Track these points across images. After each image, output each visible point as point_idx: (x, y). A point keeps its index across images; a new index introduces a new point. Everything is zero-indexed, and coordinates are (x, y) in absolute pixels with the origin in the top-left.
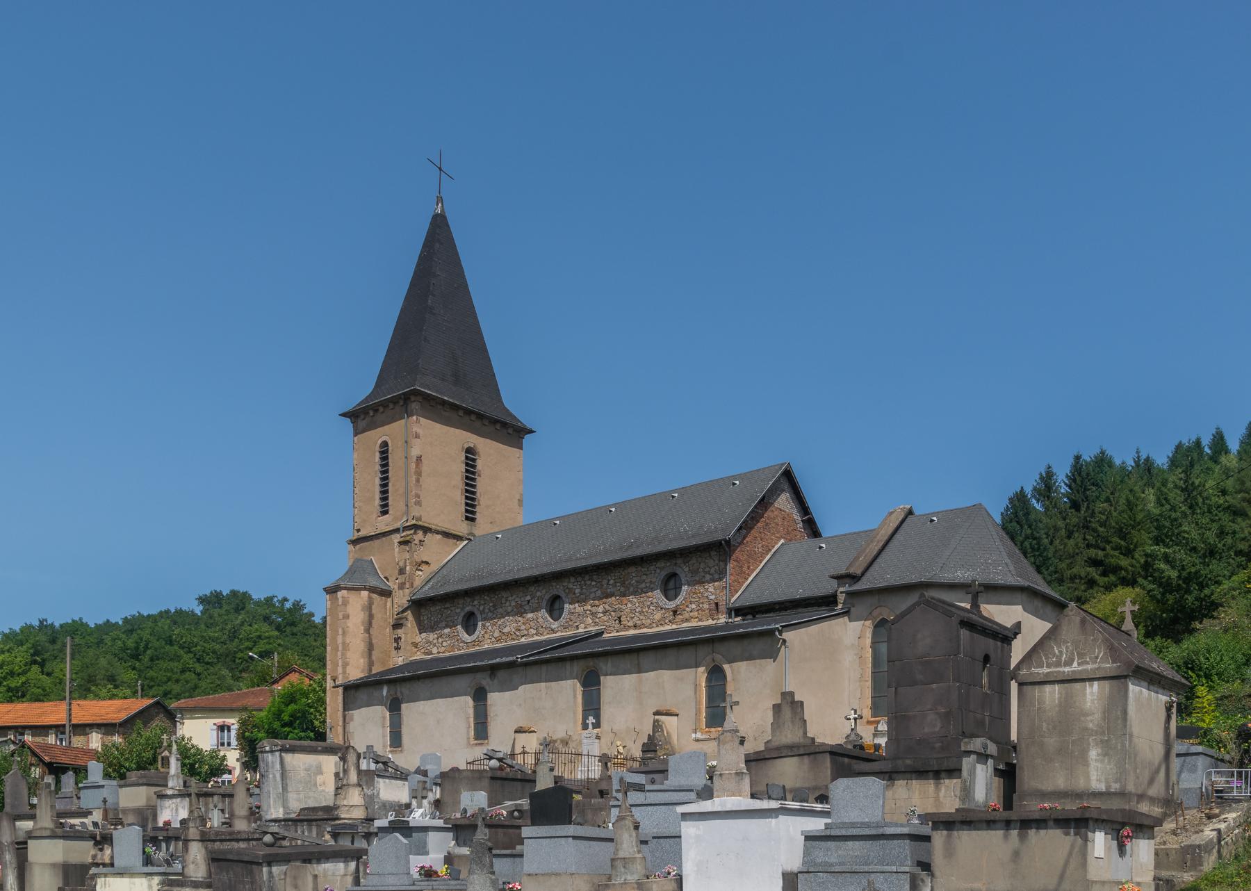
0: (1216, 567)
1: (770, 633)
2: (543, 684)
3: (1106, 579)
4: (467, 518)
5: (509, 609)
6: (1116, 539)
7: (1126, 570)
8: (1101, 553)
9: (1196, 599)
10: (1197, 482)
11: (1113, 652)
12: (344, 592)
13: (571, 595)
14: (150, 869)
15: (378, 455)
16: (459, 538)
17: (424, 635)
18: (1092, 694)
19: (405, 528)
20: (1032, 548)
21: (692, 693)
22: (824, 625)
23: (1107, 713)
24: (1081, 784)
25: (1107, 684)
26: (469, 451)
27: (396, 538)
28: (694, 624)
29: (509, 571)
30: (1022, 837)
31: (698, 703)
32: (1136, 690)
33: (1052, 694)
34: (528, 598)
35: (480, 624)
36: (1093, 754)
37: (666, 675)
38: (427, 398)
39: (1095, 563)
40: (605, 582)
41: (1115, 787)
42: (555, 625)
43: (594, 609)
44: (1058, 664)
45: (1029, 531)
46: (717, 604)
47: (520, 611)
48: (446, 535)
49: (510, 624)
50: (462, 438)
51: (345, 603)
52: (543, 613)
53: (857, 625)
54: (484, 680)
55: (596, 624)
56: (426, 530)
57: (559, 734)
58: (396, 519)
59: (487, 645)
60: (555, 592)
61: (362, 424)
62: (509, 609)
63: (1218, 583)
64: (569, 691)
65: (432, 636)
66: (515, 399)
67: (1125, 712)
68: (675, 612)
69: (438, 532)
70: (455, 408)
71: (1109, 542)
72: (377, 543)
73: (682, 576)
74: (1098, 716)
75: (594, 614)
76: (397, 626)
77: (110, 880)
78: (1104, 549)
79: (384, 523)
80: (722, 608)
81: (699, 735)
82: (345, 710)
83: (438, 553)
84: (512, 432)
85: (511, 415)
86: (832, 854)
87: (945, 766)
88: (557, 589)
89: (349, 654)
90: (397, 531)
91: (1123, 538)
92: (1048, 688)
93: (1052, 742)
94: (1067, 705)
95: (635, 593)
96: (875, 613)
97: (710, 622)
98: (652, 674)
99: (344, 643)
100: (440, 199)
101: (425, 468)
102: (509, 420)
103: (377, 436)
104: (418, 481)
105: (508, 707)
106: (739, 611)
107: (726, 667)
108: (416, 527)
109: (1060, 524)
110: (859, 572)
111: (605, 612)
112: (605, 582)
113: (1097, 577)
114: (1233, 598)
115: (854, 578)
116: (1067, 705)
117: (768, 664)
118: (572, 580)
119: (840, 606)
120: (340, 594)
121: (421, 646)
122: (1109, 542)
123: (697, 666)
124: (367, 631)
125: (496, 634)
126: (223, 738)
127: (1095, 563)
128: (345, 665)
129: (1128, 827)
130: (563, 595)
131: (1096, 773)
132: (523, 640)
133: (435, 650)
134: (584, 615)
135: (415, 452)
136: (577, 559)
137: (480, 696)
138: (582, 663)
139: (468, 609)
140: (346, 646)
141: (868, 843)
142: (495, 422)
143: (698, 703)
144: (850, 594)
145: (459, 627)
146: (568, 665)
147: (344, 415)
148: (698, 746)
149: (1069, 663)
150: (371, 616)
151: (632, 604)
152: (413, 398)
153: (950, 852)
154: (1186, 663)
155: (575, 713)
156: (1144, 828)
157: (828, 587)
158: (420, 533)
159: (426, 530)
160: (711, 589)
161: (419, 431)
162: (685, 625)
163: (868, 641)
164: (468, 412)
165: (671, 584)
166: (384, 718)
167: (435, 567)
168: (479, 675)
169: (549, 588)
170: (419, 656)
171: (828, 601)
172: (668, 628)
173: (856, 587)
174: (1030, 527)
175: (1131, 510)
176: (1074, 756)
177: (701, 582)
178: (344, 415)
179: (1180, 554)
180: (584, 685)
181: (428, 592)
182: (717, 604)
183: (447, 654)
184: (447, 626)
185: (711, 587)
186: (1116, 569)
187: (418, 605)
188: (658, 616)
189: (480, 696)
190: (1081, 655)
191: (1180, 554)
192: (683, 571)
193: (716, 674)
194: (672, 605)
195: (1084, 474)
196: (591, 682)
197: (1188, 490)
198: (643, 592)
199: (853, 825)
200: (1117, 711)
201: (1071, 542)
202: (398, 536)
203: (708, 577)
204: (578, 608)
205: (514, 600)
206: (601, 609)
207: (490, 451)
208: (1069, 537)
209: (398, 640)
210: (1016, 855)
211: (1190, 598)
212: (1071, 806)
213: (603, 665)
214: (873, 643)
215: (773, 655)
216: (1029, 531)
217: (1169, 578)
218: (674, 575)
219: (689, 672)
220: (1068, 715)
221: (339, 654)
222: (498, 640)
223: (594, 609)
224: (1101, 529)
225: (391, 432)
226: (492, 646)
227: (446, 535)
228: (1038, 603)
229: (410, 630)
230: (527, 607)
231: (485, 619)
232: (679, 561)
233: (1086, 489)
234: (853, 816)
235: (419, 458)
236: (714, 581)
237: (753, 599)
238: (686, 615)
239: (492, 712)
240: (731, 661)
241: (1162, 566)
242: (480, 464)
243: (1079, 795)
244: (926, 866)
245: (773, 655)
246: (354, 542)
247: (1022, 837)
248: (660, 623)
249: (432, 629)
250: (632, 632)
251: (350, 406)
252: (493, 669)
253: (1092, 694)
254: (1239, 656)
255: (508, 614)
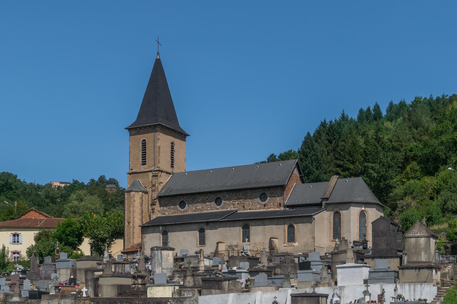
0: (391, 172)
1: (311, 216)
2: (228, 228)
3: (344, 173)
4: (172, 167)
5: (199, 201)
6: (347, 157)
7: (353, 170)
8: (342, 162)
9: (384, 184)
10: (381, 136)
11: (427, 231)
12: (133, 192)
13: (225, 198)
14: (169, 284)
15: (141, 145)
16: (170, 174)
17: (162, 208)
18: (422, 240)
19: (154, 171)
20: (315, 160)
21: (283, 233)
22: (321, 213)
23: (426, 244)
24: (420, 260)
25: (426, 238)
26: (172, 143)
27: (150, 174)
28: (272, 209)
29: (199, 188)
30: (419, 271)
31: (285, 235)
32: (432, 239)
33: (413, 240)
34: (207, 198)
35: (187, 205)
36: (423, 253)
37: (274, 227)
38: (162, 126)
39: (339, 166)
40: (238, 194)
41: (428, 260)
42: (218, 207)
43: (234, 203)
44: (415, 233)
45: (314, 153)
46: (280, 204)
47: (204, 202)
48: (167, 173)
49: (199, 206)
50: (171, 139)
51: (134, 196)
52: (214, 203)
53: (329, 213)
54: (204, 226)
55: (234, 207)
56: (162, 171)
57: (234, 243)
58: (149, 167)
59: (190, 213)
60: (218, 196)
61: (133, 132)
62: (199, 201)
63: (391, 178)
64: (238, 231)
65: (165, 208)
66: (183, 125)
67: (430, 244)
68: (265, 205)
69: (165, 172)
70: (169, 129)
71: (345, 158)
72: (141, 175)
73: (268, 195)
74: (424, 245)
75: (234, 205)
76: (153, 204)
77: (155, 288)
78: (343, 161)
79: (143, 168)
80: (282, 205)
81: (285, 245)
82: (142, 234)
83: (164, 179)
84: (182, 136)
85: (182, 130)
86: (374, 275)
87: (387, 256)
88: (220, 195)
89: (135, 214)
90: (151, 171)
91: (351, 157)
92: (412, 239)
93: (413, 251)
94: (416, 242)
95: (250, 199)
96: (335, 209)
97: (278, 209)
98: (269, 226)
99: (133, 210)
100: (158, 54)
101: (161, 150)
102: (182, 132)
103: (142, 137)
104: (159, 155)
105: (212, 235)
106: (288, 206)
107: (295, 225)
108: (159, 171)
109: (325, 149)
110: (328, 197)
111: (238, 204)
112: (238, 194)
113: (340, 172)
114: (398, 185)
115: (327, 199)
116: (416, 242)
117: (309, 225)
118: (225, 193)
119: (323, 207)
120: (131, 193)
121: (160, 212)
122: (345, 158)
123: (285, 224)
124: (141, 206)
125: (194, 209)
126: (15, 239)
127: (339, 166)
128: (134, 218)
129: (438, 269)
130: (222, 198)
131: (423, 258)
132: (205, 211)
133: (167, 213)
134: (230, 204)
135: (158, 144)
136: (227, 186)
137: (202, 231)
138: (243, 222)
139: (182, 200)
140: (134, 211)
141: (384, 273)
142: (179, 133)
143: (285, 235)
144: (326, 204)
145: (178, 206)
146: (237, 223)
147: (126, 129)
148: (285, 248)
149: (417, 233)
150: (142, 201)
151: (248, 202)
152: (158, 126)
153: (403, 274)
154: (405, 220)
155: (240, 237)
156: (439, 269)
157: (319, 201)
158: (160, 172)
159: (162, 171)
160: (278, 199)
161: (160, 137)
162: (269, 209)
163: (332, 217)
164: (172, 130)
165: (263, 196)
166: (160, 237)
167: (164, 184)
168: (202, 224)
169: (217, 196)
170: (160, 215)
171: (320, 205)
172: (262, 210)
173: (328, 202)
174: (314, 151)
175: (354, 146)
176: (418, 254)
177: (274, 197)
178: (126, 129)
179: (377, 166)
180: (243, 229)
181: (163, 193)
182: (280, 204)
183: (172, 215)
184: (172, 205)
185: (278, 198)
186: (348, 169)
187: (160, 198)
188: (258, 206)
189: (202, 231)
190: (420, 232)
191: (377, 166)
192: (268, 193)
193: (291, 227)
194: (264, 203)
195: (333, 129)
196: (246, 228)
197: (378, 140)
198: (252, 198)
199: (381, 269)
200: (428, 244)
201: (329, 157)
202: (151, 173)
203: (277, 195)
204: (228, 202)
205: (201, 198)
206: (236, 203)
207: (177, 141)
208: (328, 155)
209: (153, 209)
210: (418, 274)
211: (382, 184)
212: (417, 265)
213: (250, 223)
214: (333, 218)
215: (311, 222)
216: (314, 153)
217: (374, 176)
218: (264, 194)
219: (282, 227)
220: (417, 245)
221: (131, 214)
222: (194, 211)
223: (234, 203)
224: (342, 153)
225: (148, 137)
226: (191, 213)
227: (167, 173)
228: (379, 207)
229: (157, 207)
230: (207, 201)
231: (189, 204)
232: (266, 190)
233: (334, 135)
234: (381, 267)
235: (160, 147)
236: (279, 196)
237: (292, 203)
238: (269, 207)
239: (207, 236)
240: (297, 223)
241: (372, 172)
242: (175, 147)
243: (420, 262)
244: (398, 277)
245: (311, 222)
246: (130, 174)
247: (419, 271)
248: (259, 208)
249: (166, 206)
250: (249, 211)
251: (128, 125)
252: (207, 223)
253: (422, 240)
254: (420, 217)
255: (199, 203)
